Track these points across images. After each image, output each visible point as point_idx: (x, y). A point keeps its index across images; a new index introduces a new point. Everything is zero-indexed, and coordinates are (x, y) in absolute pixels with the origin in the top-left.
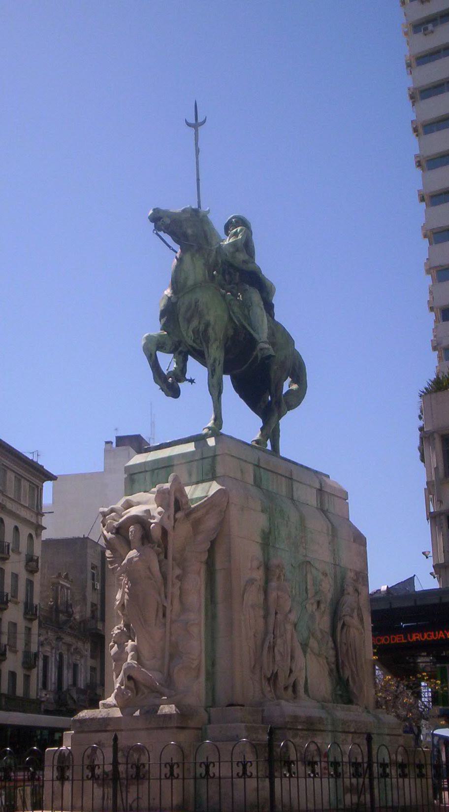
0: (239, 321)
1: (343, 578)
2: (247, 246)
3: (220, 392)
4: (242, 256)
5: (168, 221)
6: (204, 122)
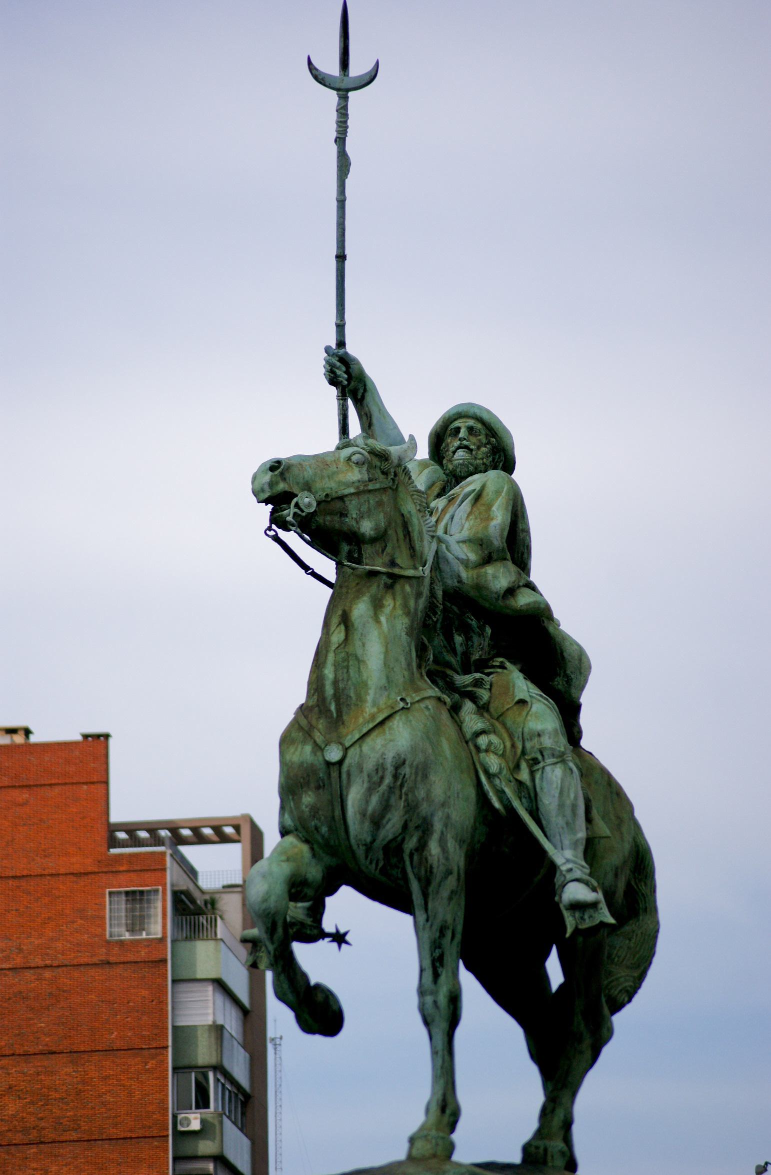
0: (500, 793)
1: (269, 897)
2: (515, 545)
3: (454, 1020)
4: (499, 577)
5: (307, 501)
6: (371, 77)
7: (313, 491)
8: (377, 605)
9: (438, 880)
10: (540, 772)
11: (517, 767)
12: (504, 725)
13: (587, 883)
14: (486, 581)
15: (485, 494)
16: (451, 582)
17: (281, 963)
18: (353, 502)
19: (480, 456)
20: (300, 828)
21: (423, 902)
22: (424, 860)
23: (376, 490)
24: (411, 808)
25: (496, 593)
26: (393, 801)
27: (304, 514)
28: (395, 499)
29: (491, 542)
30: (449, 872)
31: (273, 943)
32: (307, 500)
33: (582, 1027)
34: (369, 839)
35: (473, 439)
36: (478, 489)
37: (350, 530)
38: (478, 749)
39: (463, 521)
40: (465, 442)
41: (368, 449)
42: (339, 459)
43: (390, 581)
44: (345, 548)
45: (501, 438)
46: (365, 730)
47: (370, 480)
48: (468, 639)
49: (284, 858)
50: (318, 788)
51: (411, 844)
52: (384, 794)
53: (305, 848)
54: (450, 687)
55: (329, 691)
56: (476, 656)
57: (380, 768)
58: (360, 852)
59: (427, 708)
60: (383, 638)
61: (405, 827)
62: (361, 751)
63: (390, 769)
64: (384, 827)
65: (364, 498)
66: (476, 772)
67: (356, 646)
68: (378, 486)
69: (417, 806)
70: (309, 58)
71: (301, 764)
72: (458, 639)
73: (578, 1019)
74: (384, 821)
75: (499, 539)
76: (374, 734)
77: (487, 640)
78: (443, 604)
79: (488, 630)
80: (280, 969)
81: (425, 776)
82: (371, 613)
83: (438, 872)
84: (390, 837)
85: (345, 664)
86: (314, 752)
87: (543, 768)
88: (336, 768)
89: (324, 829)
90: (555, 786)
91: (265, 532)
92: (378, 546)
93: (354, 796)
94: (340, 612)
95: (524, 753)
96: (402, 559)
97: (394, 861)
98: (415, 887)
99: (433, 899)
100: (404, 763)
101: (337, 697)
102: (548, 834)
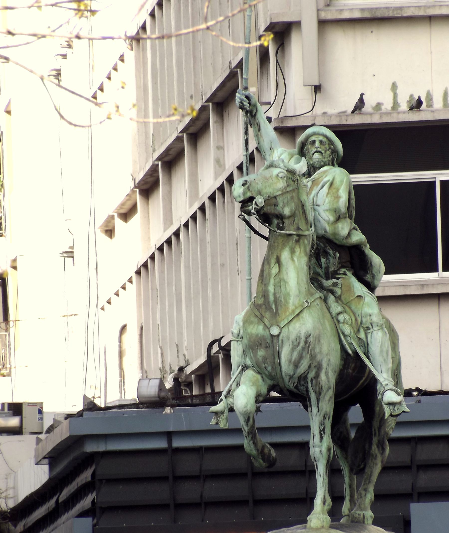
0: (350, 344)
7: (262, 194)
8: (293, 252)
9: (324, 392)
10: (371, 333)
11: (359, 330)
12: (350, 308)
13: (394, 391)
14: (338, 231)
15: (335, 182)
16: (321, 232)
17: (251, 436)
18: (281, 199)
19: (326, 156)
20: (255, 366)
21: (317, 403)
22: (318, 383)
23: (290, 191)
24: (313, 357)
25: (343, 236)
26: (304, 354)
27: (259, 208)
28: (298, 193)
29: (340, 210)
30: (329, 388)
31: (247, 426)
32: (260, 200)
33: (377, 451)
34: (292, 374)
35: (323, 147)
36: (331, 179)
37: (279, 213)
38: (339, 321)
39: (325, 198)
40: (319, 149)
41: (286, 169)
42: (272, 175)
43: (297, 238)
44: (275, 221)
45: (336, 146)
46: (290, 319)
47: (288, 186)
48: (327, 259)
49: (251, 384)
50: (266, 347)
51: (312, 375)
52: (300, 351)
53: (259, 377)
54: (321, 287)
55: (271, 298)
56: (332, 269)
57: (298, 338)
58: (287, 379)
59: (317, 304)
60: (294, 269)
61: (310, 367)
62: (289, 329)
63: (303, 339)
64: (300, 367)
65: (285, 196)
66: (339, 335)
67: (284, 275)
68: (291, 188)
69: (315, 357)
70: (362, 95)
71: (257, 335)
72: (323, 260)
73: (374, 447)
74: (300, 365)
75: (344, 208)
76: (294, 321)
77: (337, 260)
78: (316, 243)
79: (338, 255)
80: (250, 438)
81: (319, 341)
82: (290, 256)
83: (325, 388)
84: (303, 372)
85: (279, 284)
86: (264, 329)
88: (276, 338)
89: (269, 368)
90: (378, 341)
91: (239, 217)
92: (291, 220)
93: (285, 352)
94: (275, 257)
95: (361, 323)
96: (303, 226)
97: (302, 382)
98: (313, 396)
99: (322, 402)
100: (310, 335)
101: (276, 301)
102: (374, 365)
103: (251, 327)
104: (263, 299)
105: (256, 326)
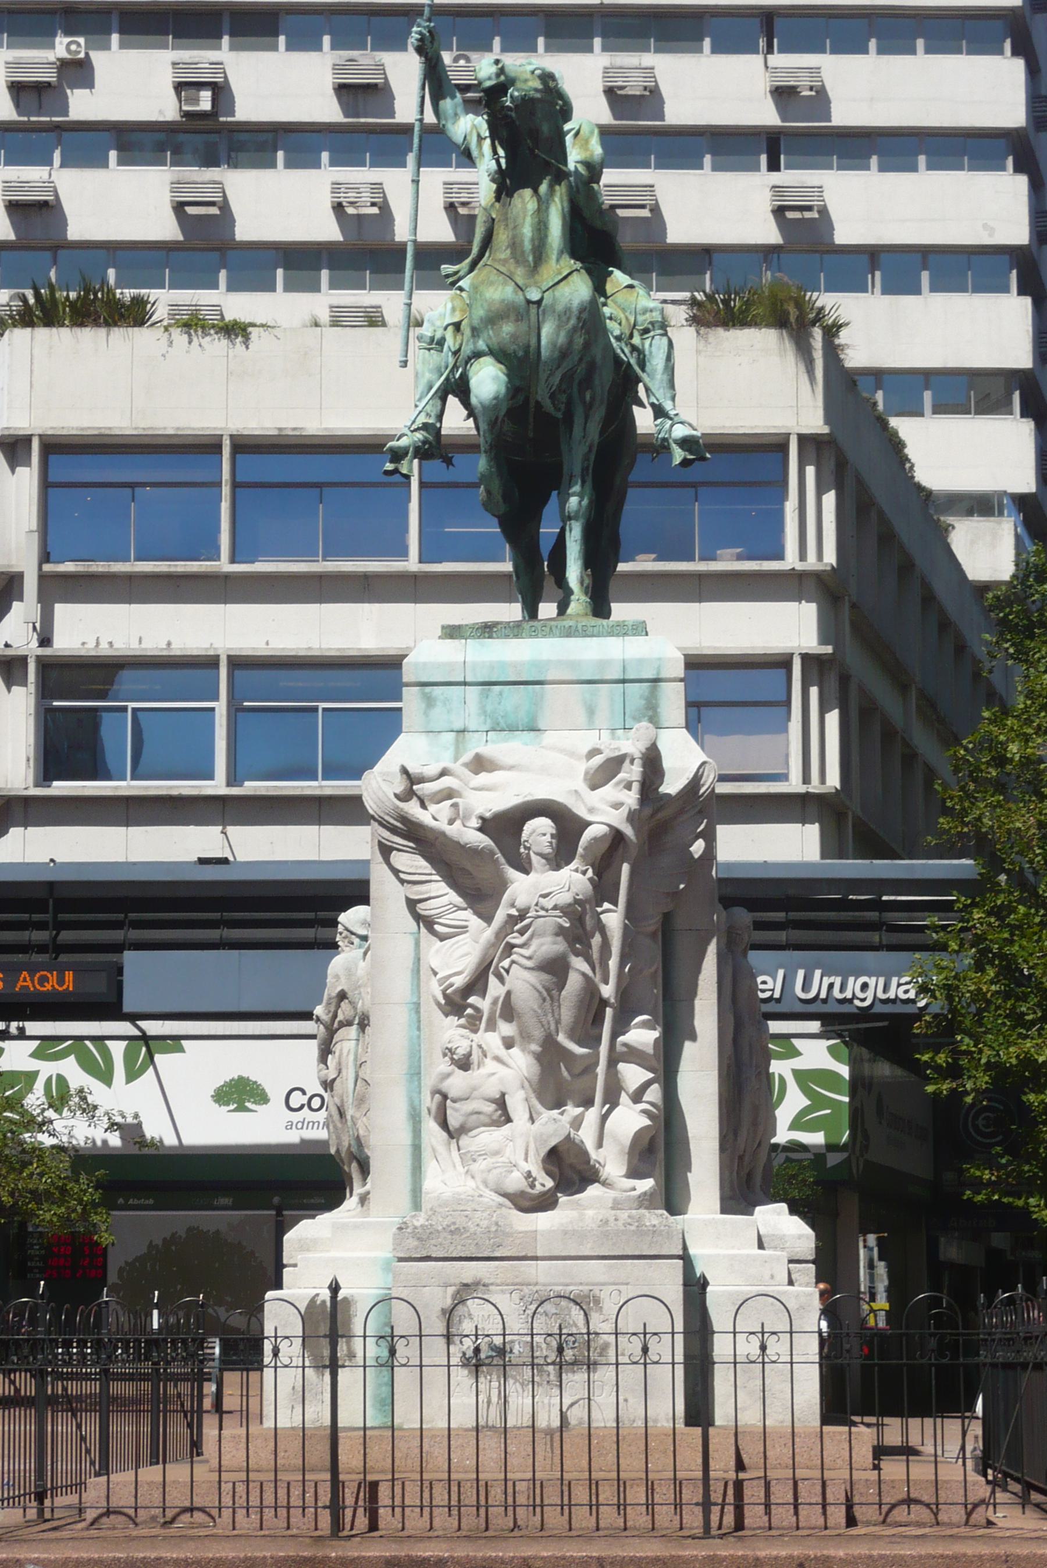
15: (582, 132)
46: (556, 280)
50: (517, 320)
86: (516, 293)
87: (653, 337)
93: (547, 331)
103: (492, 289)
104: (508, 251)
105: (500, 288)
